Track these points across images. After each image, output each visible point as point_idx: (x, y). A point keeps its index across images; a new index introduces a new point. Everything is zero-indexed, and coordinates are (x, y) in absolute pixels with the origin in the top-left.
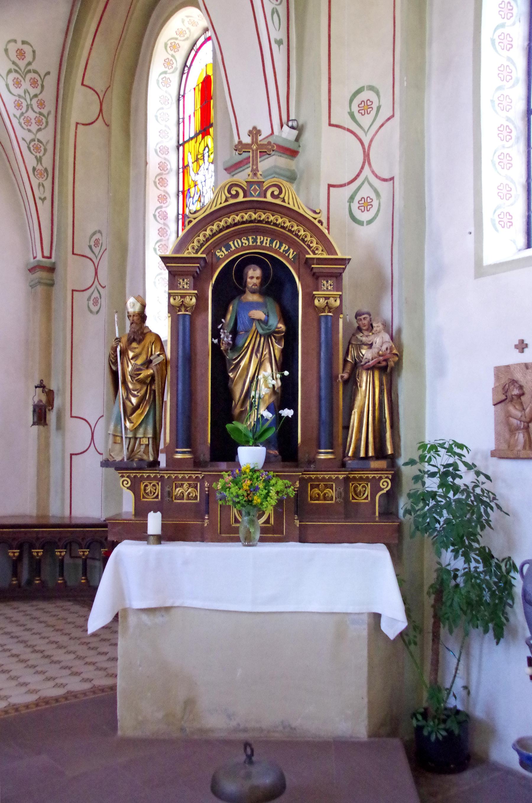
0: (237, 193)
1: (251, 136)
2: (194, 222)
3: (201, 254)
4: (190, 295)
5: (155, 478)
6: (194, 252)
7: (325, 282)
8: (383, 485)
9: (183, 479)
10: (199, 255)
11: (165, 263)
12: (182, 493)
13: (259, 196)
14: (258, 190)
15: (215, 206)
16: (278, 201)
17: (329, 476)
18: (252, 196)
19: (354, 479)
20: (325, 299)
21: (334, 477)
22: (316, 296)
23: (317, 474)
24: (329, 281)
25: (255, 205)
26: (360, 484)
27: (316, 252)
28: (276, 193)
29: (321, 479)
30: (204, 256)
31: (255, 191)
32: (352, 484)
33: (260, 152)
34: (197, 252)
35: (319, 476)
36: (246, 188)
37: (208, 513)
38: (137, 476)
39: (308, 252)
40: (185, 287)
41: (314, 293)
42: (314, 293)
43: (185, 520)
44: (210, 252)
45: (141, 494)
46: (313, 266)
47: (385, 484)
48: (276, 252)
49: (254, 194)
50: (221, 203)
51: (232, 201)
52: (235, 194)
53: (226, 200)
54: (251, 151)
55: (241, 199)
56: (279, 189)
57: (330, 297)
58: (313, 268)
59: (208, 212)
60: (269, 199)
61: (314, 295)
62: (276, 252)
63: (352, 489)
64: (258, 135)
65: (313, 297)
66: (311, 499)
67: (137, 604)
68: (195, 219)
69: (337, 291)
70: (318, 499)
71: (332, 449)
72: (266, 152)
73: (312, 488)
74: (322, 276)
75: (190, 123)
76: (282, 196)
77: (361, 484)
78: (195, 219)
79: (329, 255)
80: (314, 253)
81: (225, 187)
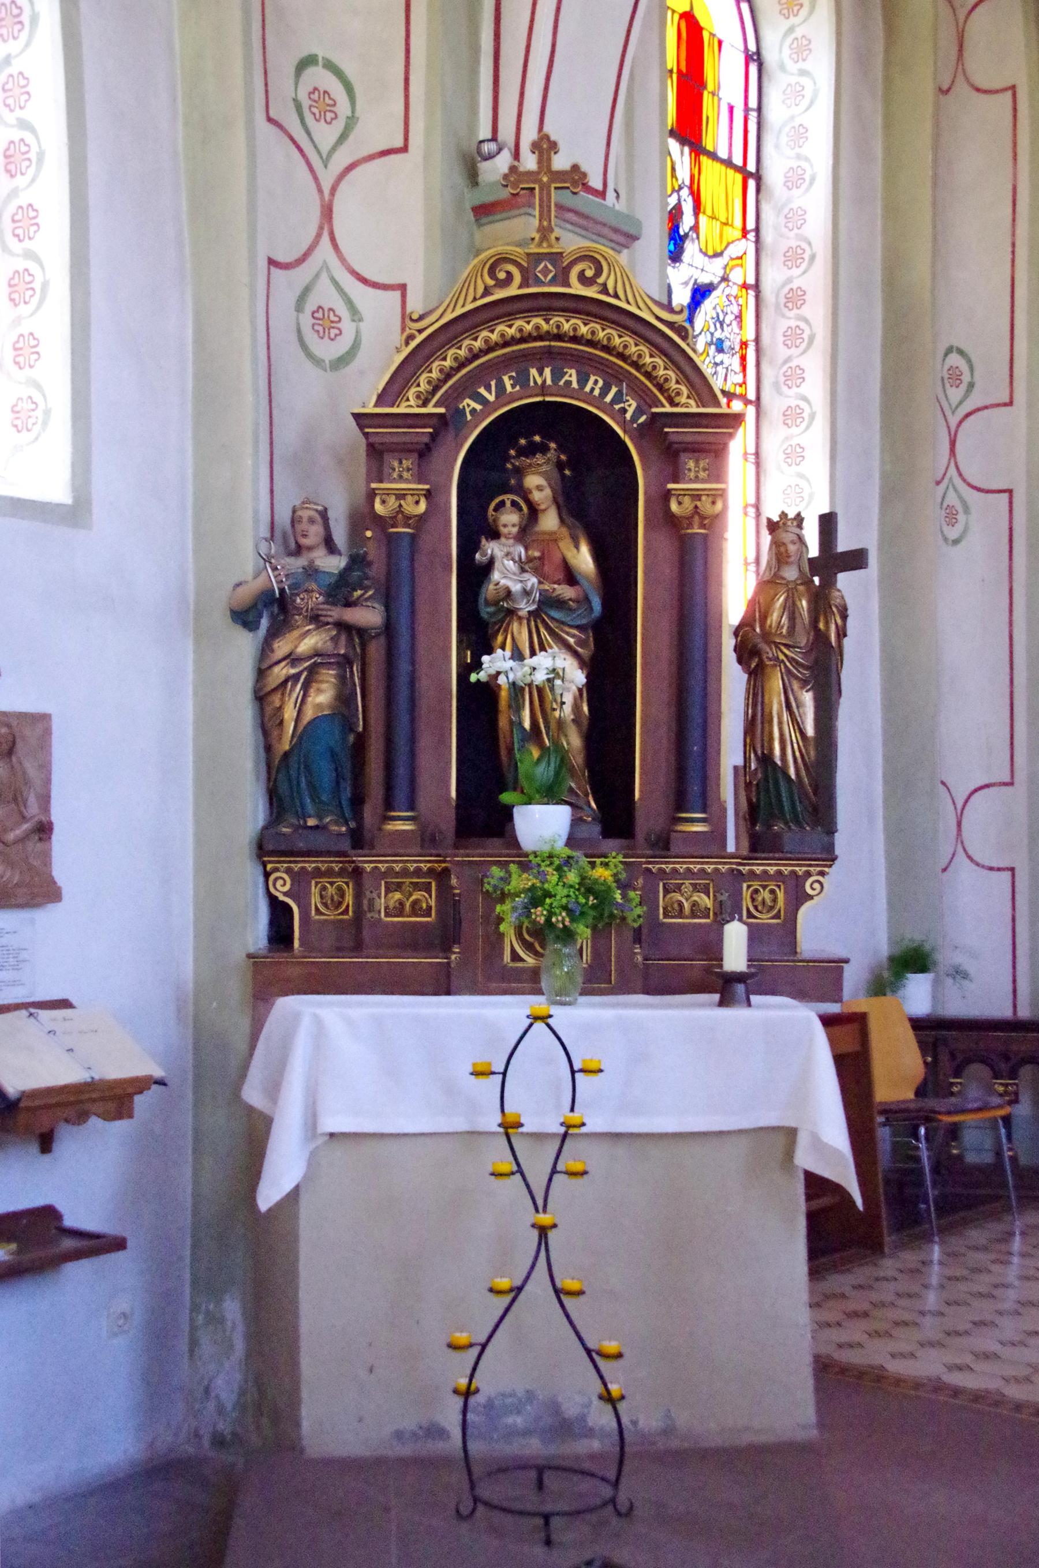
0: (509, 275)
1: (537, 152)
2: (420, 338)
3: (435, 406)
4: (413, 492)
5: (342, 873)
6: (420, 402)
7: (396, 464)
8: (813, 889)
9: (405, 873)
10: (430, 409)
11: (361, 427)
12: (401, 903)
13: (553, 282)
14: (539, 272)
15: (463, 306)
16: (591, 292)
17: (313, 865)
18: (539, 282)
19: (752, 874)
20: (396, 499)
21: (710, 868)
22: (673, 492)
23: (753, 864)
24: (404, 462)
25: (544, 303)
26: (332, 884)
27: (677, 400)
28: (589, 273)
29: (774, 875)
30: (442, 410)
31: (545, 271)
32: (749, 887)
33: (556, 188)
34: (425, 404)
35: (692, 866)
36: (526, 265)
37: (640, 943)
38: (392, 868)
39: (660, 401)
40: (405, 475)
41: (670, 486)
42: (670, 486)
43: (314, 955)
44: (451, 400)
45: (310, 904)
46: (666, 430)
47: (817, 886)
48: (598, 402)
49: (542, 278)
50: (475, 299)
51: (500, 294)
52: (587, 278)
53: (487, 292)
54: (537, 187)
55: (513, 291)
56: (593, 263)
57: (701, 495)
58: (667, 433)
59: (449, 317)
60: (577, 289)
61: (669, 490)
62: (598, 402)
63: (746, 894)
64: (552, 153)
65: (667, 495)
66: (666, 916)
67: (595, 1124)
68: (420, 331)
69: (419, 483)
70: (681, 914)
71: (704, 811)
72: (568, 188)
73: (667, 891)
74: (685, 450)
75: (731, 128)
76: (601, 280)
77: (335, 882)
78: (420, 331)
79: (704, 406)
80: (673, 404)
81: (485, 263)
